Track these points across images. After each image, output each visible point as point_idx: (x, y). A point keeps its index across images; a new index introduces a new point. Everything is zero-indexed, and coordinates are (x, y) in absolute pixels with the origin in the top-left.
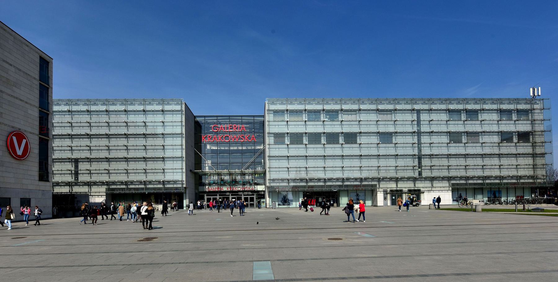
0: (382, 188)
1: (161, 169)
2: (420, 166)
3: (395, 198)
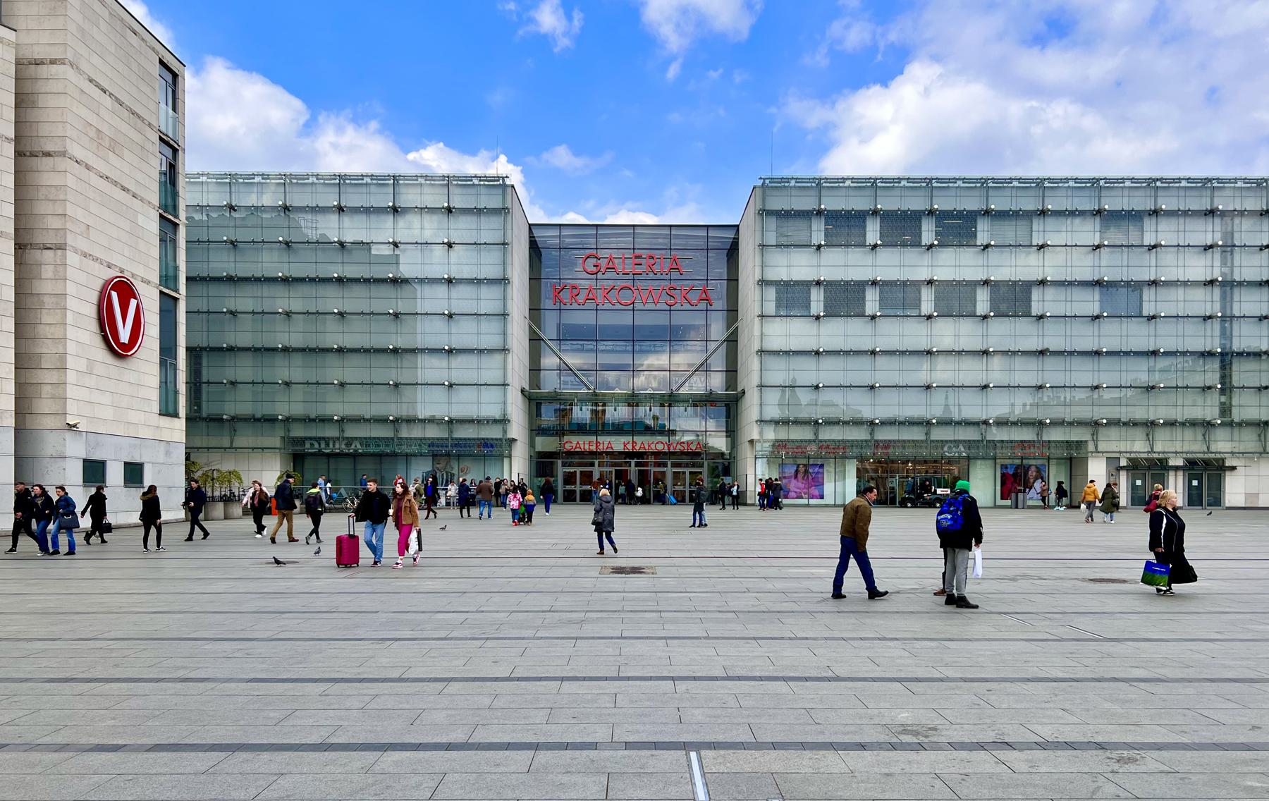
0: (1103, 453)
1: (280, 382)
2: (1227, 388)
3: (1200, 483)
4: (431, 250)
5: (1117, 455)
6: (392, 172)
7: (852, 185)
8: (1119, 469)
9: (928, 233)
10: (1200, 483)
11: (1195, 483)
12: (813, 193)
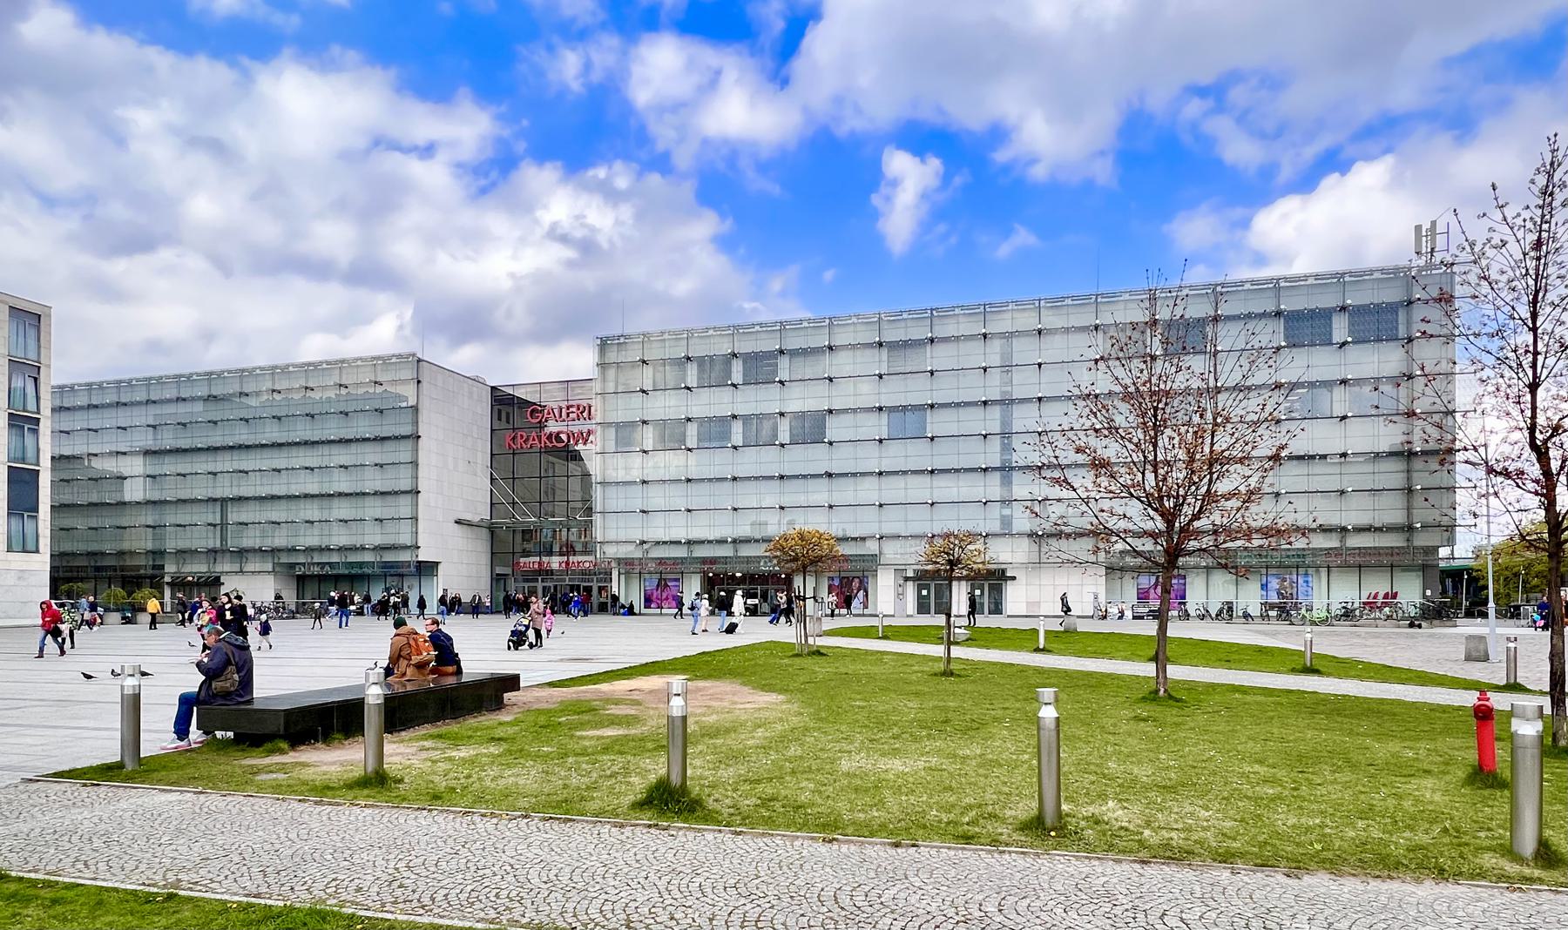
3: (929, 592)
4: (264, 424)
5: (903, 567)
6: (685, 327)
7: (1252, 287)
8: (907, 579)
9: (1340, 329)
10: (929, 592)
11: (924, 592)
12: (1271, 294)
